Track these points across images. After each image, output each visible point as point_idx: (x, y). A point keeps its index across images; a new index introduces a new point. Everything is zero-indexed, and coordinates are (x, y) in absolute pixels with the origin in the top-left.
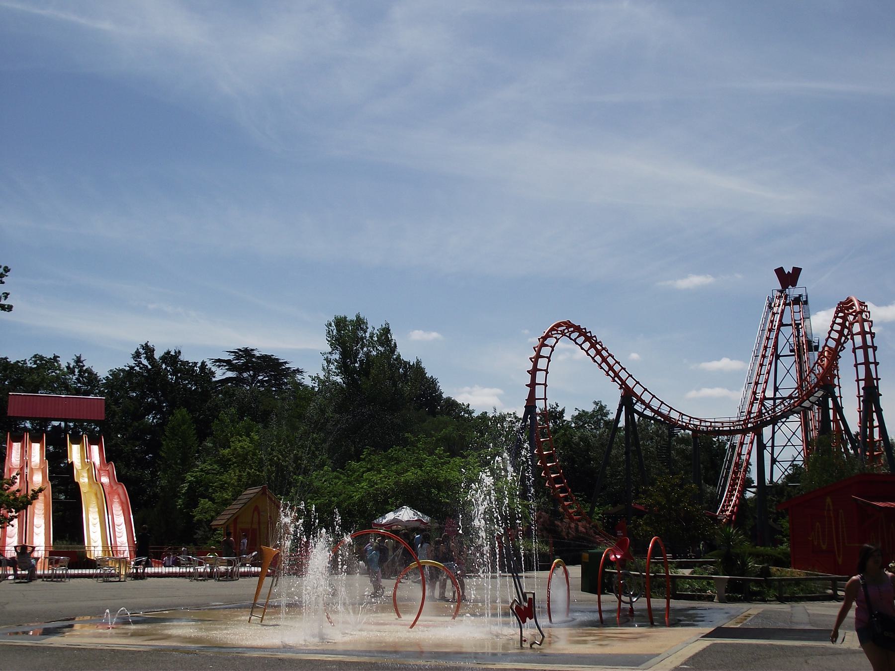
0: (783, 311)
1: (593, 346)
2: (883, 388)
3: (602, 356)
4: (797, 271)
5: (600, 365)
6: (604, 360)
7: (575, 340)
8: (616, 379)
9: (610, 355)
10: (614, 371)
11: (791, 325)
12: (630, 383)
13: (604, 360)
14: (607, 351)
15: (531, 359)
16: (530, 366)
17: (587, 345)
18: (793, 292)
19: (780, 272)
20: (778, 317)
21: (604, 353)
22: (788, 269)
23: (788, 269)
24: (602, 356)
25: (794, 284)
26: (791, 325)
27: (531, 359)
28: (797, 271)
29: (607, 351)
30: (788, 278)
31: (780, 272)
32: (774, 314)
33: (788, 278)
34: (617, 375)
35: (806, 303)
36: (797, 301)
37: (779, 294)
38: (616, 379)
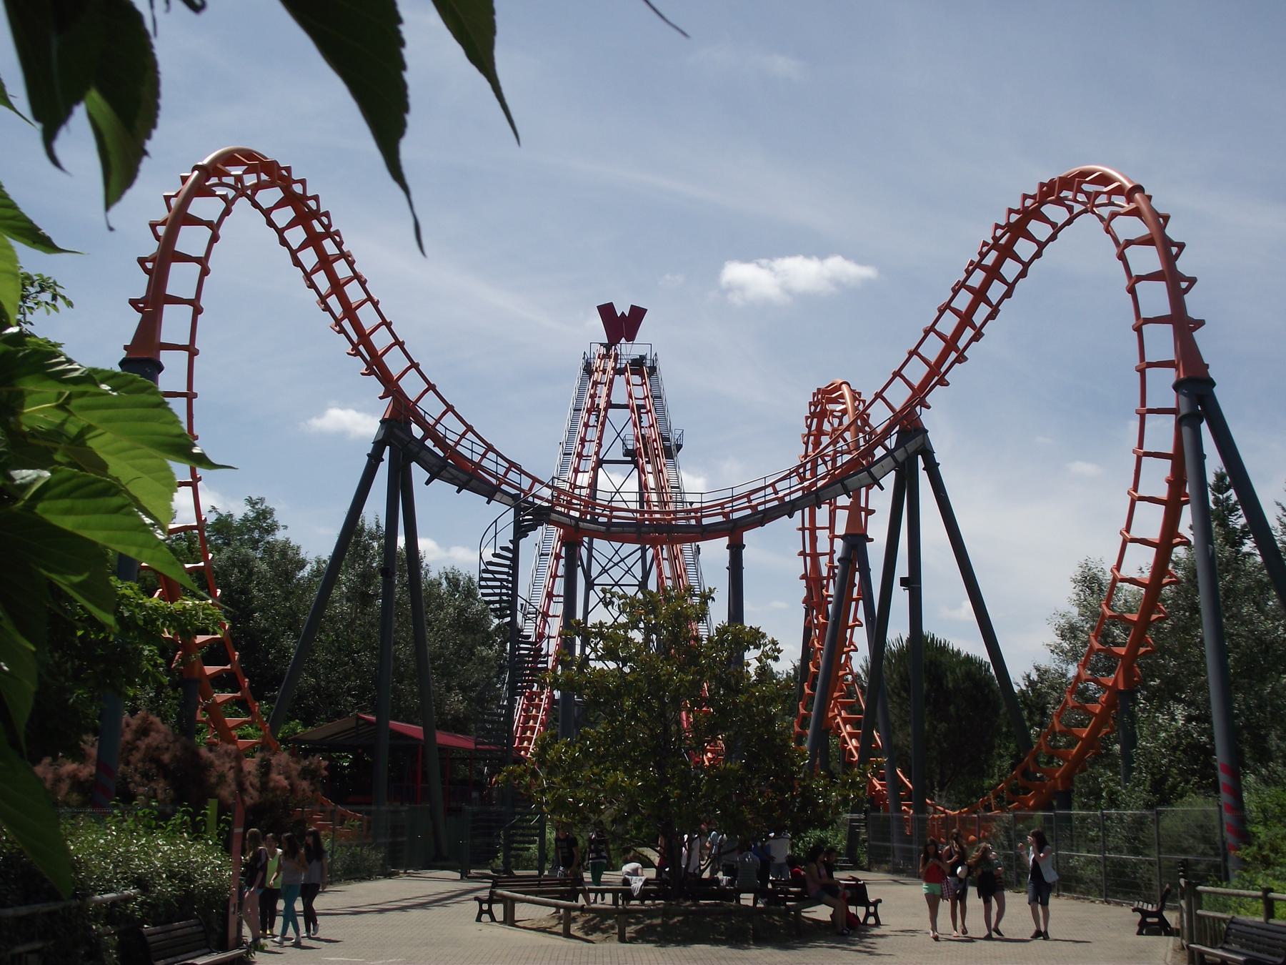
0: (611, 381)
1: (313, 240)
2: (470, 498)
3: (332, 276)
4: (638, 314)
5: (308, 276)
6: (337, 287)
7: (267, 213)
8: (361, 348)
9: (357, 276)
10: (343, 300)
11: (626, 407)
12: (411, 386)
13: (325, 263)
14: (351, 264)
15: (142, 261)
16: (139, 285)
17: (297, 236)
18: (628, 351)
19: (607, 311)
20: (602, 391)
21: (341, 269)
22: (622, 309)
23: (622, 309)
24: (332, 276)
25: (631, 338)
26: (626, 407)
27: (142, 261)
28: (638, 314)
29: (351, 264)
30: (621, 325)
31: (607, 311)
32: (596, 384)
33: (621, 325)
34: (350, 311)
35: (653, 370)
36: (638, 365)
37: (603, 351)
38: (346, 324)
